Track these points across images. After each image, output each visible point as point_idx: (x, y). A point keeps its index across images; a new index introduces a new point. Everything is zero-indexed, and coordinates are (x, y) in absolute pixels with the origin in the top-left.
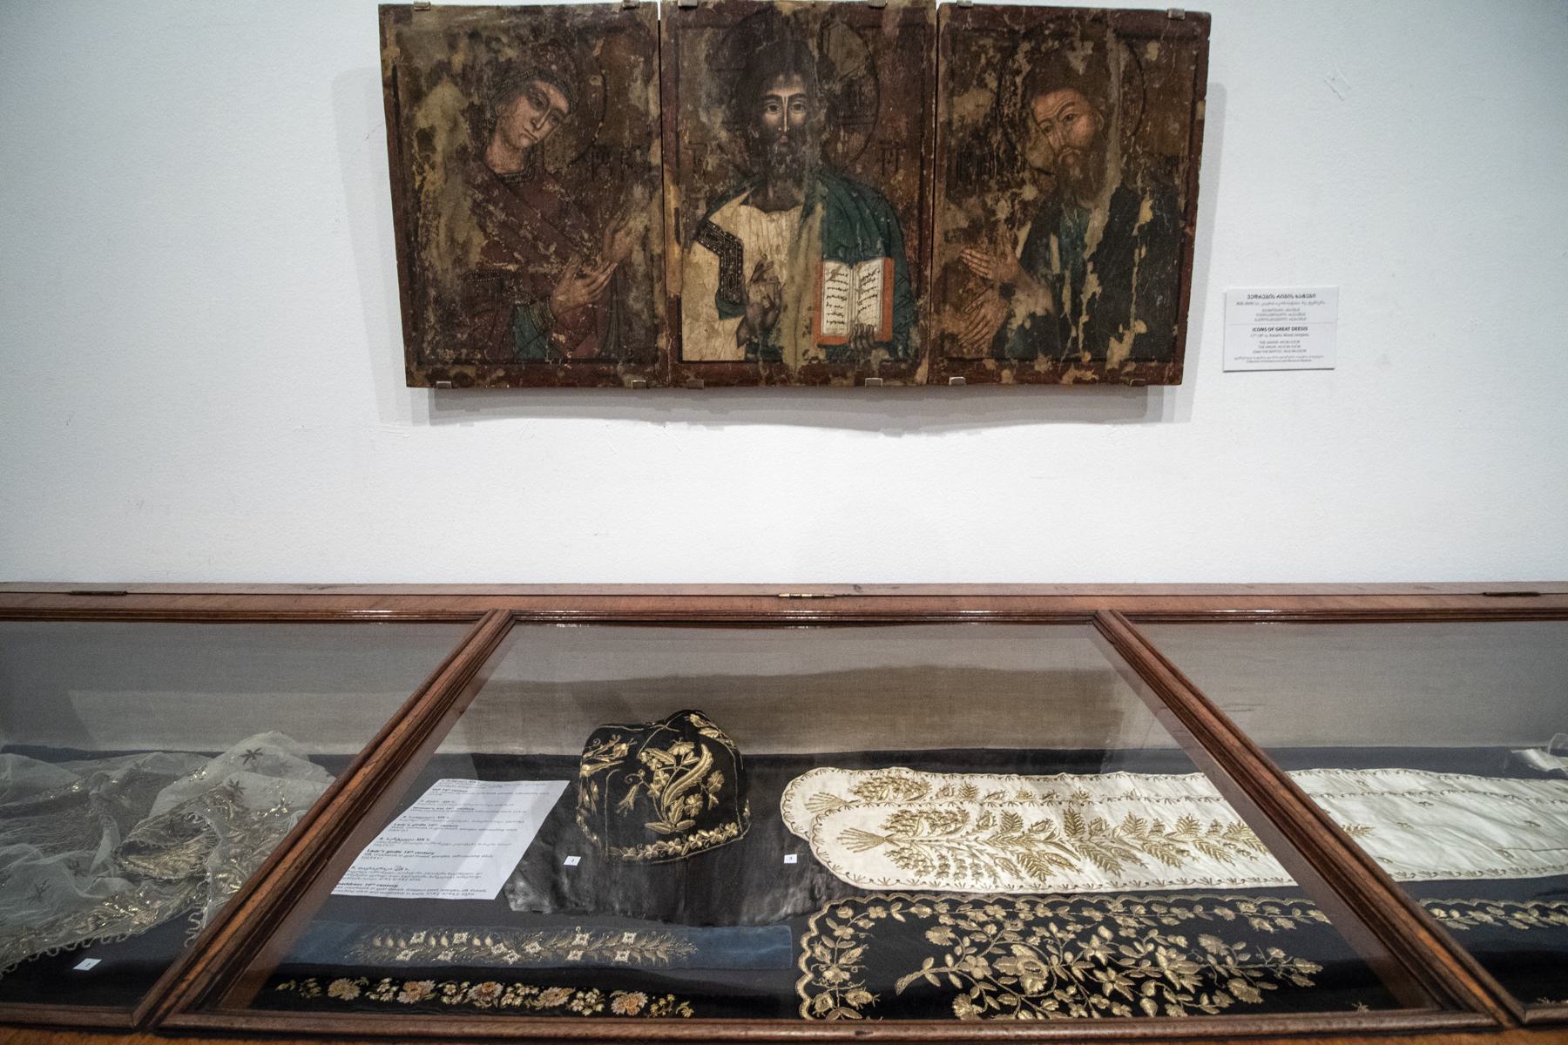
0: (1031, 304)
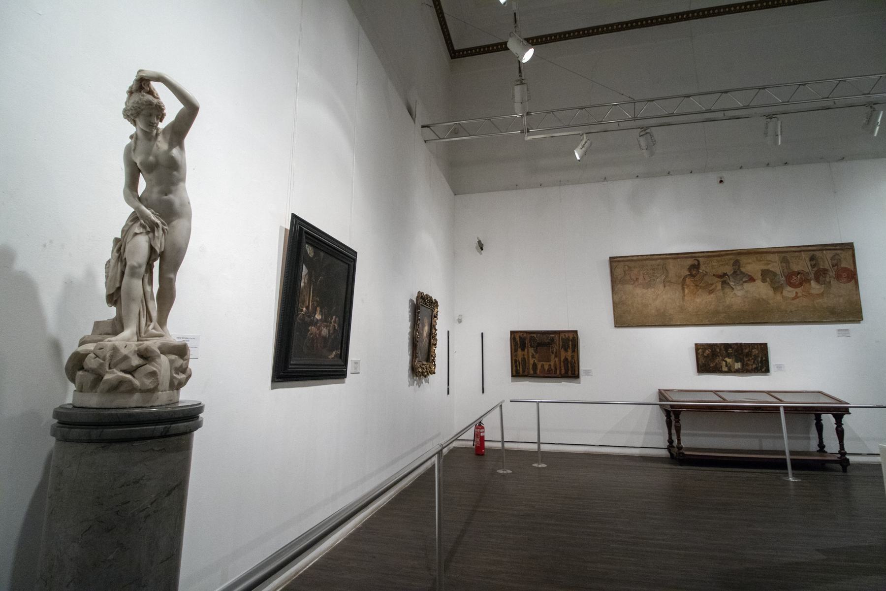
0: (754, 366)
